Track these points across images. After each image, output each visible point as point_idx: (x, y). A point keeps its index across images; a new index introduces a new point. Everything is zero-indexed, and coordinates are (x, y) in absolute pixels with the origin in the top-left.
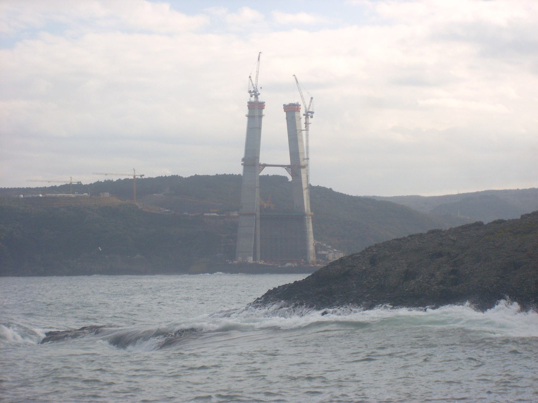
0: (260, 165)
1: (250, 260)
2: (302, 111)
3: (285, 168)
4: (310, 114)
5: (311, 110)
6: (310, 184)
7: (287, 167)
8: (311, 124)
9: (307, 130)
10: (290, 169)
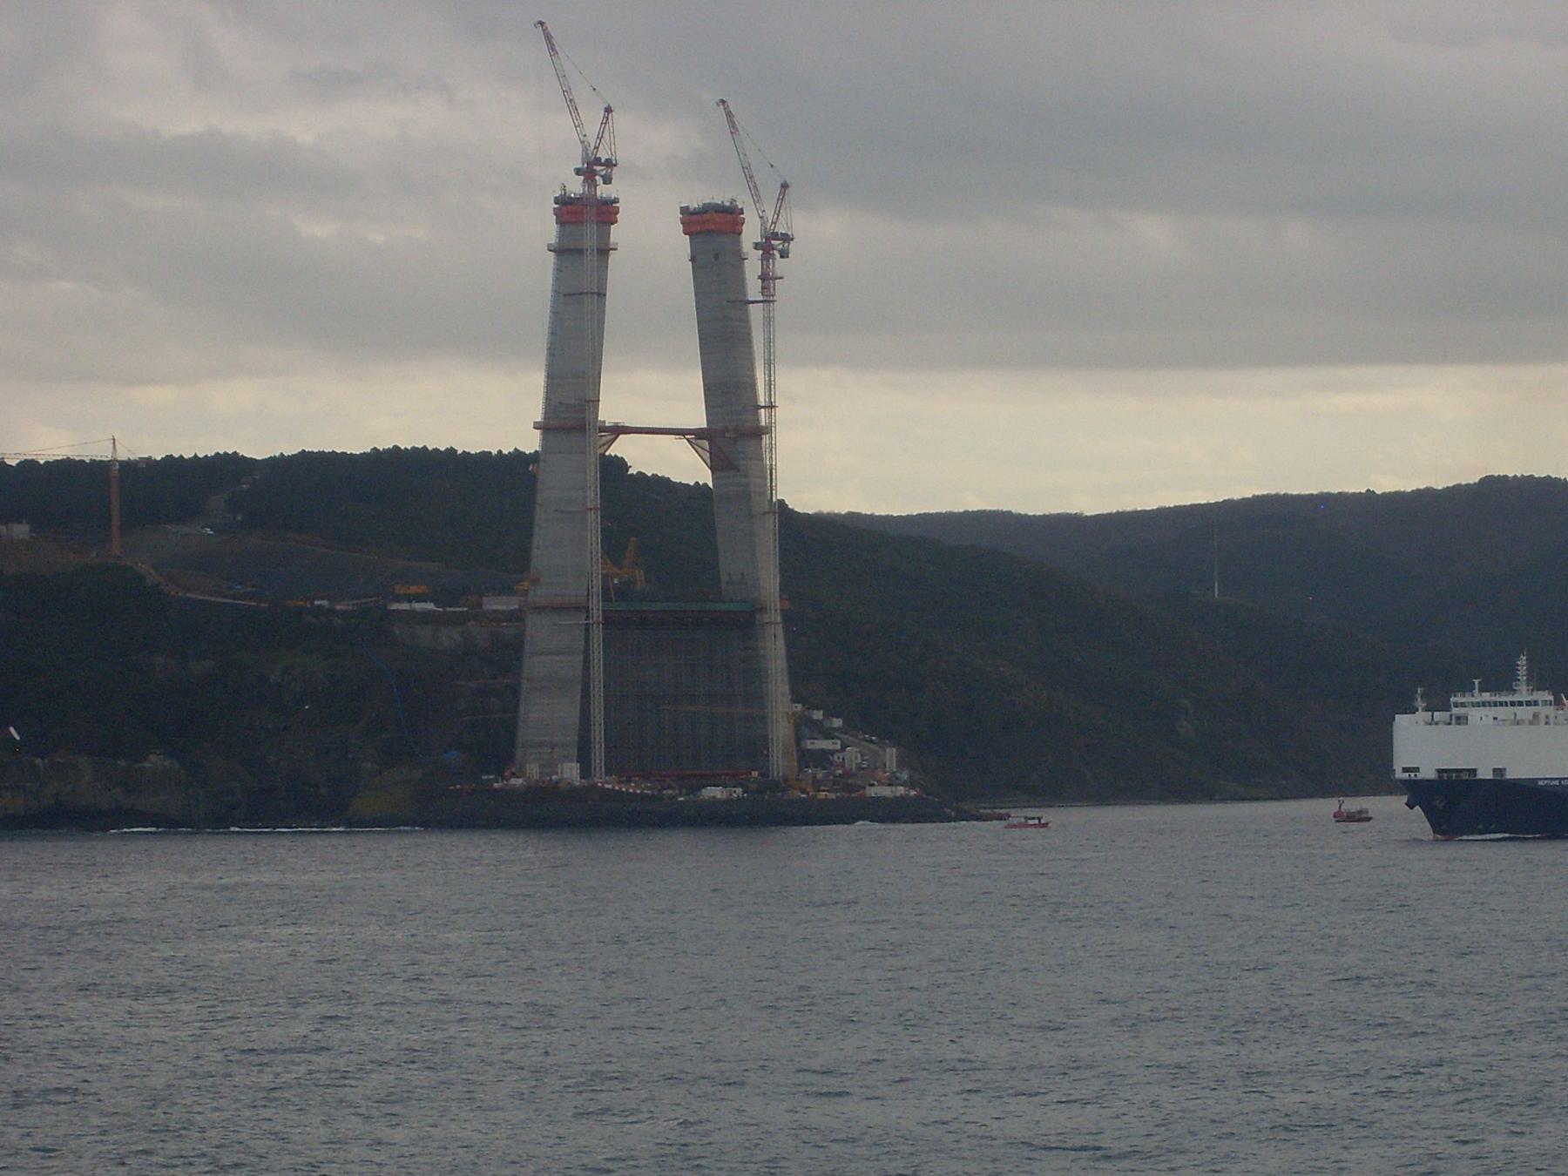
0: (604, 429)
1: (570, 772)
2: (751, 233)
3: (688, 440)
4: (603, 168)
5: (603, 155)
6: (781, 503)
7: (694, 436)
8: (781, 278)
9: (768, 300)
10: (706, 444)
